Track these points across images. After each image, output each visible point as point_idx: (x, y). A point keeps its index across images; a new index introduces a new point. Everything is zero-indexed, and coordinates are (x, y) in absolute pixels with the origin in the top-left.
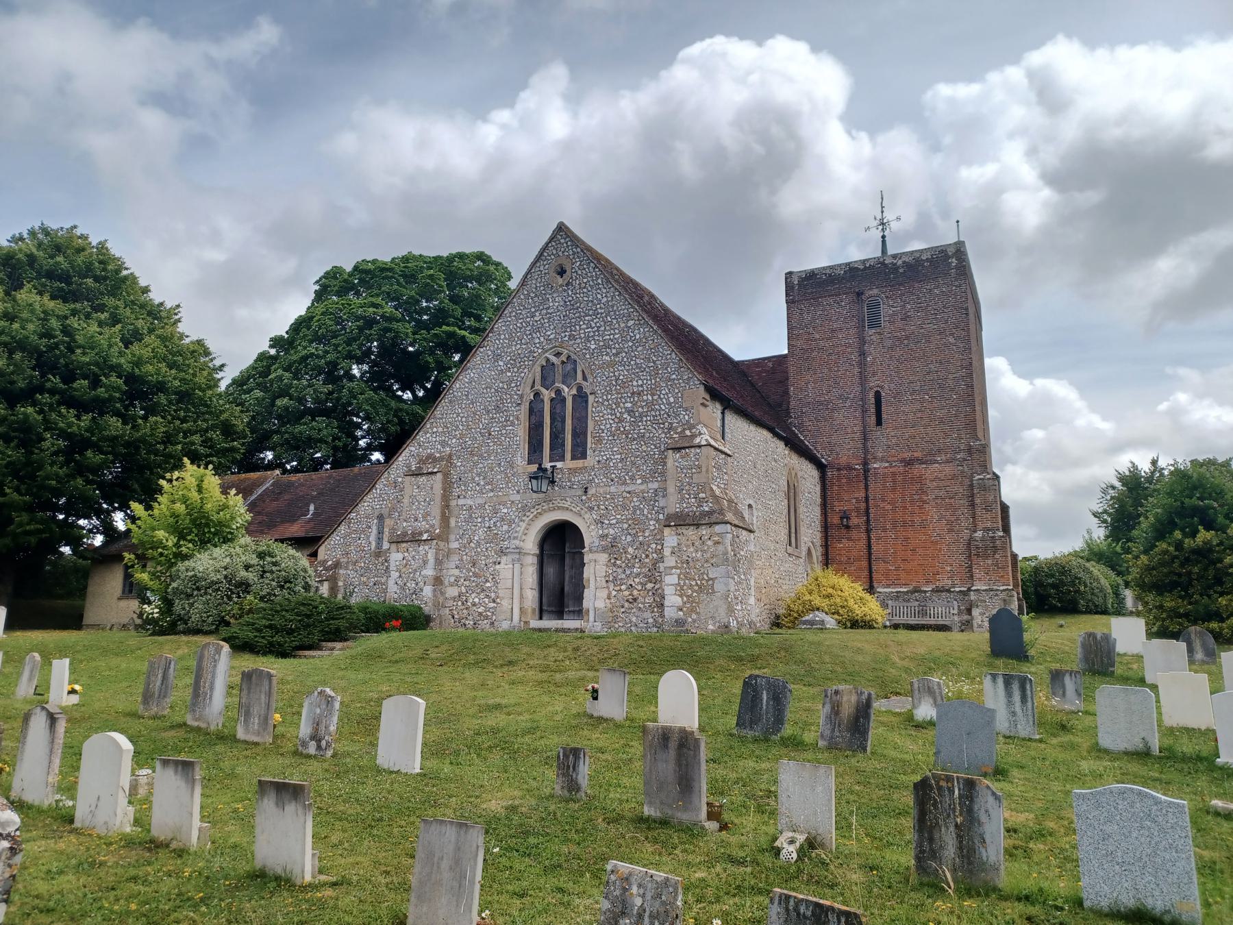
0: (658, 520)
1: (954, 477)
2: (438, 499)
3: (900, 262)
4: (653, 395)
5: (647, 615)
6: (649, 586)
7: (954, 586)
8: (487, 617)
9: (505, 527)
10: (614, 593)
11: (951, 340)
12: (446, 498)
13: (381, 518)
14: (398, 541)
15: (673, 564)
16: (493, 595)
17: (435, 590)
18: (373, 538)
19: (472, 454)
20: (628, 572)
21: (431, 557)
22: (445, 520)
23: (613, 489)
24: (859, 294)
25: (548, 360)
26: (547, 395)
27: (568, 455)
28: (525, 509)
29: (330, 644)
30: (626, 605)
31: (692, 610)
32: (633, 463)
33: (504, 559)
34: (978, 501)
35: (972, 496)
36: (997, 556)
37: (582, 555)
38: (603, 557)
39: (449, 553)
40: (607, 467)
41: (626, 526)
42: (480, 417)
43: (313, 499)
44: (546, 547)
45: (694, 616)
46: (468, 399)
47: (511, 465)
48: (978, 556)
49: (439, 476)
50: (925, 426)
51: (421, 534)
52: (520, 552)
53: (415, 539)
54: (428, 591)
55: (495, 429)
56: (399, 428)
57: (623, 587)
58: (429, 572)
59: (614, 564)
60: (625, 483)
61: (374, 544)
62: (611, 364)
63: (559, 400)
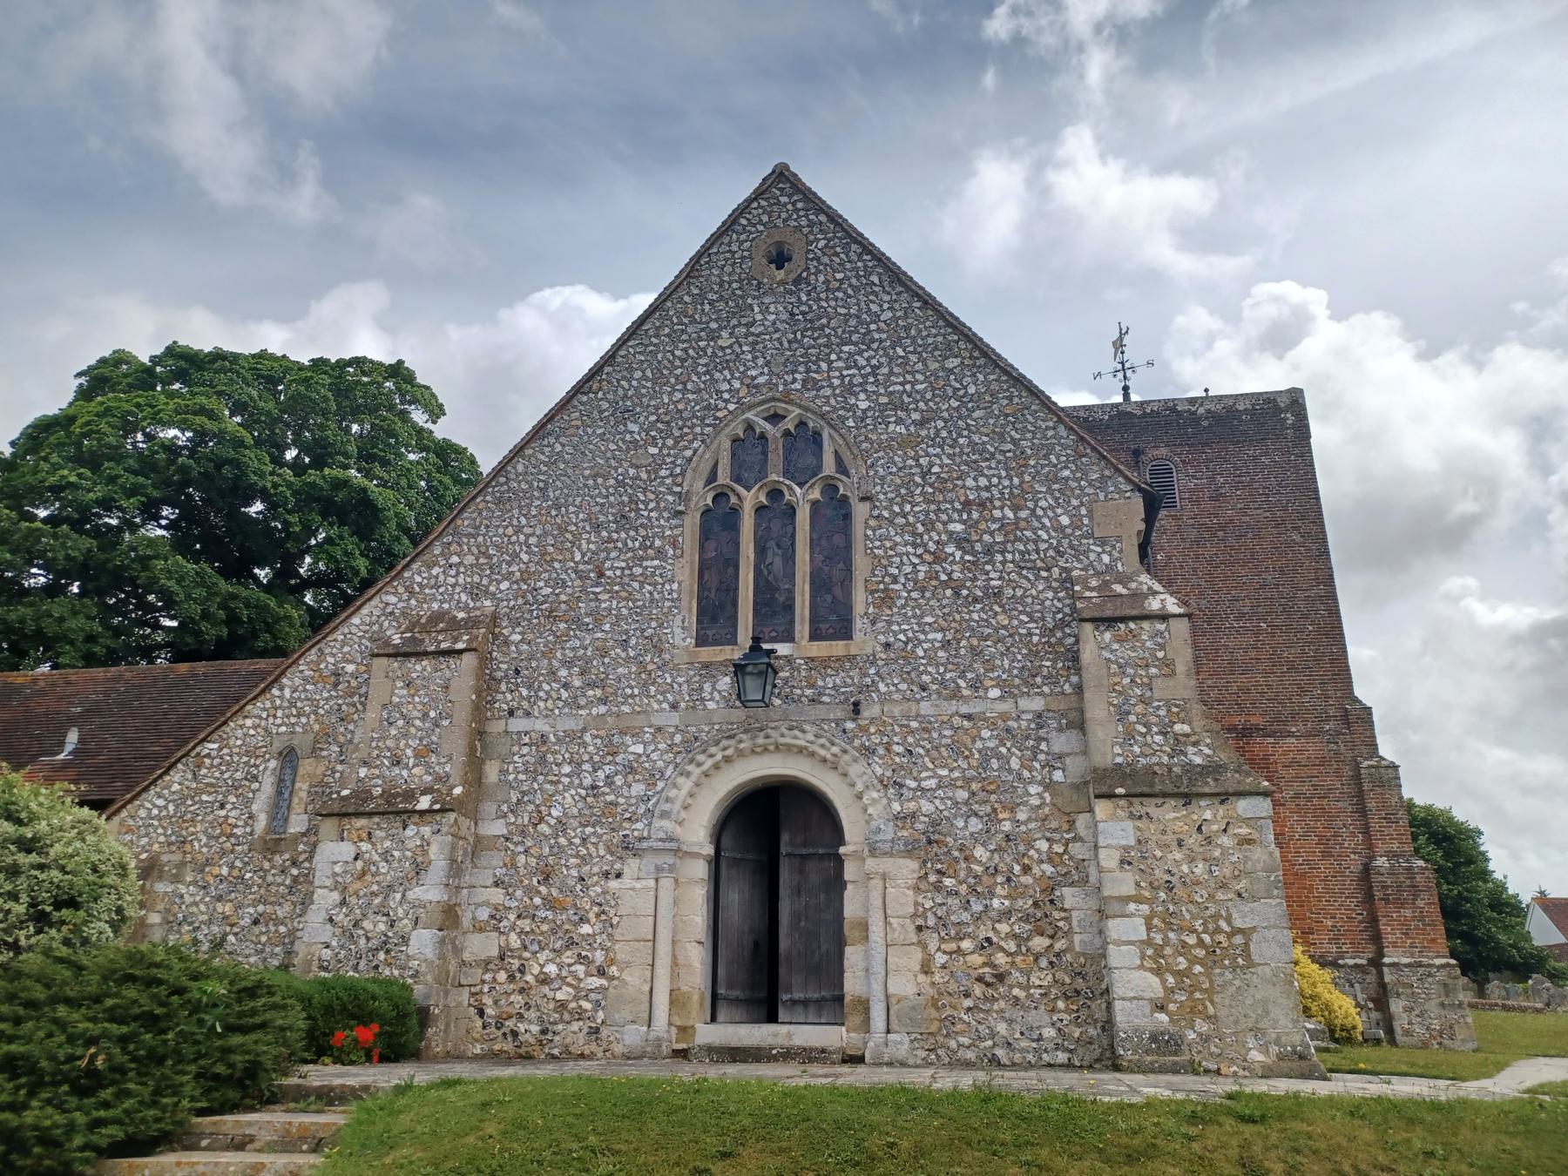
0: (1049, 786)
1: (1323, 762)
2: (462, 714)
3: (1201, 411)
4: (1016, 508)
5: (1039, 1017)
6: (1039, 943)
7: (1342, 955)
8: (580, 1015)
9: (638, 789)
10: (941, 959)
11: (1296, 537)
12: (481, 710)
13: (289, 757)
14: (344, 811)
15: (1130, 890)
16: (599, 956)
17: (442, 942)
18: (260, 806)
19: (551, 615)
20: (977, 907)
21: (437, 853)
22: (475, 765)
23: (925, 708)
24: (1137, 453)
25: (750, 427)
26: (750, 499)
27: (802, 628)
28: (691, 747)
29: (231, 1122)
30: (978, 990)
31: (1194, 1010)
32: (975, 652)
33: (631, 866)
34: (1371, 804)
35: (1361, 795)
36: (1420, 903)
37: (839, 861)
38: (906, 869)
39: (479, 845)
40: (909, 657)
41: (962, 795)
42: (577, 537)
43: (73, 721)
44: (726, 841)
45: (1202, 1026)
46: (545, 498)
47: (657, 645)
48: (1387, 901)
49: (469, 660)
50: (1266, 673)
51: (410, 796)
52: (680, 853)
53: (396, 808)
54: (423, 943)
55: (615, 566)
56: (225, 632)
57: (966, 945)
58: (430, 892)
59: (938, 887)
60: (956, 695)
61: (262, 822)
62: (905, 442)
63: (776, 510)
